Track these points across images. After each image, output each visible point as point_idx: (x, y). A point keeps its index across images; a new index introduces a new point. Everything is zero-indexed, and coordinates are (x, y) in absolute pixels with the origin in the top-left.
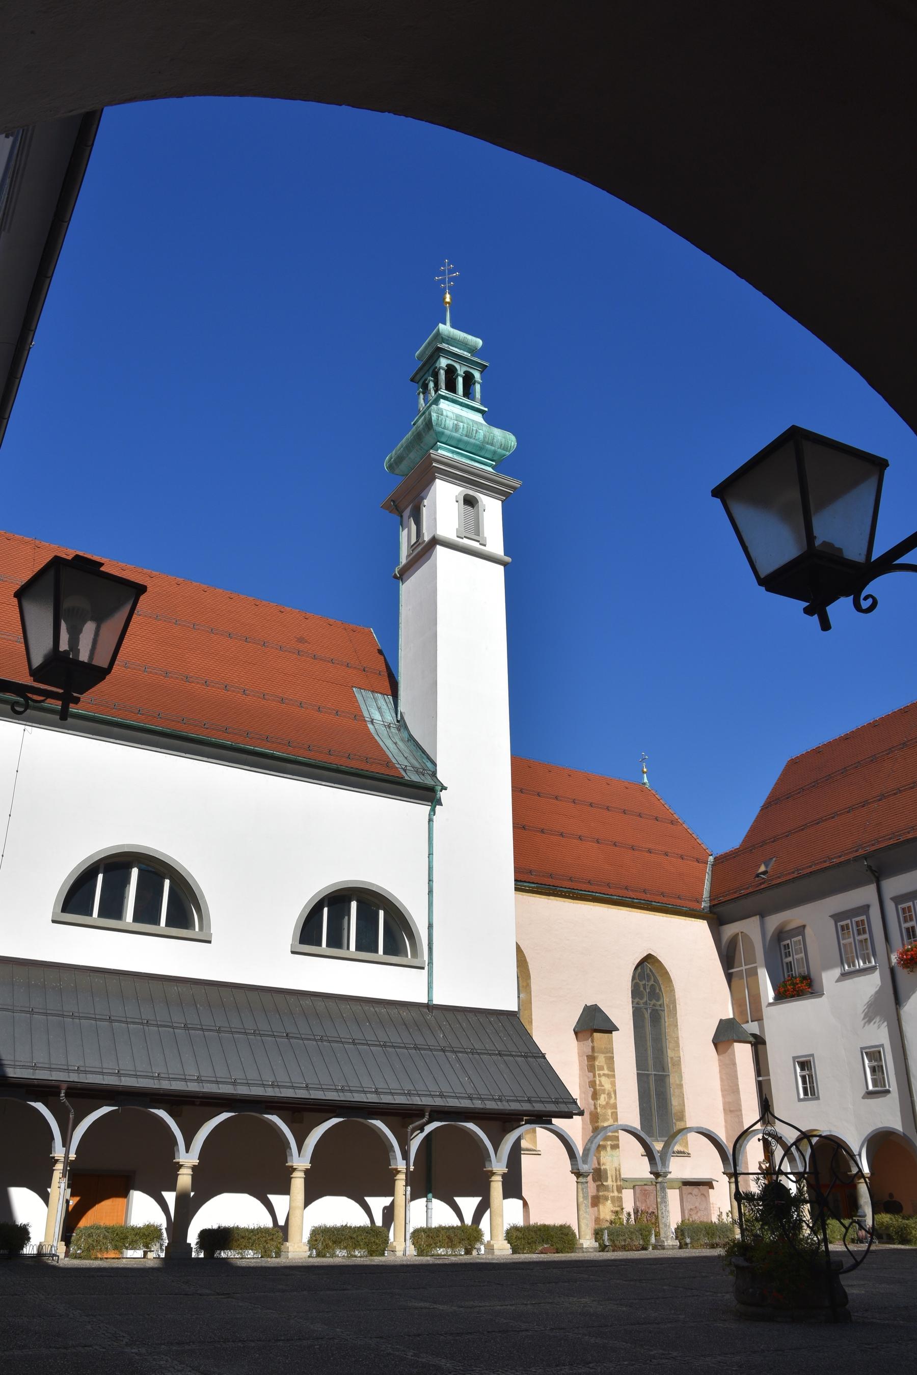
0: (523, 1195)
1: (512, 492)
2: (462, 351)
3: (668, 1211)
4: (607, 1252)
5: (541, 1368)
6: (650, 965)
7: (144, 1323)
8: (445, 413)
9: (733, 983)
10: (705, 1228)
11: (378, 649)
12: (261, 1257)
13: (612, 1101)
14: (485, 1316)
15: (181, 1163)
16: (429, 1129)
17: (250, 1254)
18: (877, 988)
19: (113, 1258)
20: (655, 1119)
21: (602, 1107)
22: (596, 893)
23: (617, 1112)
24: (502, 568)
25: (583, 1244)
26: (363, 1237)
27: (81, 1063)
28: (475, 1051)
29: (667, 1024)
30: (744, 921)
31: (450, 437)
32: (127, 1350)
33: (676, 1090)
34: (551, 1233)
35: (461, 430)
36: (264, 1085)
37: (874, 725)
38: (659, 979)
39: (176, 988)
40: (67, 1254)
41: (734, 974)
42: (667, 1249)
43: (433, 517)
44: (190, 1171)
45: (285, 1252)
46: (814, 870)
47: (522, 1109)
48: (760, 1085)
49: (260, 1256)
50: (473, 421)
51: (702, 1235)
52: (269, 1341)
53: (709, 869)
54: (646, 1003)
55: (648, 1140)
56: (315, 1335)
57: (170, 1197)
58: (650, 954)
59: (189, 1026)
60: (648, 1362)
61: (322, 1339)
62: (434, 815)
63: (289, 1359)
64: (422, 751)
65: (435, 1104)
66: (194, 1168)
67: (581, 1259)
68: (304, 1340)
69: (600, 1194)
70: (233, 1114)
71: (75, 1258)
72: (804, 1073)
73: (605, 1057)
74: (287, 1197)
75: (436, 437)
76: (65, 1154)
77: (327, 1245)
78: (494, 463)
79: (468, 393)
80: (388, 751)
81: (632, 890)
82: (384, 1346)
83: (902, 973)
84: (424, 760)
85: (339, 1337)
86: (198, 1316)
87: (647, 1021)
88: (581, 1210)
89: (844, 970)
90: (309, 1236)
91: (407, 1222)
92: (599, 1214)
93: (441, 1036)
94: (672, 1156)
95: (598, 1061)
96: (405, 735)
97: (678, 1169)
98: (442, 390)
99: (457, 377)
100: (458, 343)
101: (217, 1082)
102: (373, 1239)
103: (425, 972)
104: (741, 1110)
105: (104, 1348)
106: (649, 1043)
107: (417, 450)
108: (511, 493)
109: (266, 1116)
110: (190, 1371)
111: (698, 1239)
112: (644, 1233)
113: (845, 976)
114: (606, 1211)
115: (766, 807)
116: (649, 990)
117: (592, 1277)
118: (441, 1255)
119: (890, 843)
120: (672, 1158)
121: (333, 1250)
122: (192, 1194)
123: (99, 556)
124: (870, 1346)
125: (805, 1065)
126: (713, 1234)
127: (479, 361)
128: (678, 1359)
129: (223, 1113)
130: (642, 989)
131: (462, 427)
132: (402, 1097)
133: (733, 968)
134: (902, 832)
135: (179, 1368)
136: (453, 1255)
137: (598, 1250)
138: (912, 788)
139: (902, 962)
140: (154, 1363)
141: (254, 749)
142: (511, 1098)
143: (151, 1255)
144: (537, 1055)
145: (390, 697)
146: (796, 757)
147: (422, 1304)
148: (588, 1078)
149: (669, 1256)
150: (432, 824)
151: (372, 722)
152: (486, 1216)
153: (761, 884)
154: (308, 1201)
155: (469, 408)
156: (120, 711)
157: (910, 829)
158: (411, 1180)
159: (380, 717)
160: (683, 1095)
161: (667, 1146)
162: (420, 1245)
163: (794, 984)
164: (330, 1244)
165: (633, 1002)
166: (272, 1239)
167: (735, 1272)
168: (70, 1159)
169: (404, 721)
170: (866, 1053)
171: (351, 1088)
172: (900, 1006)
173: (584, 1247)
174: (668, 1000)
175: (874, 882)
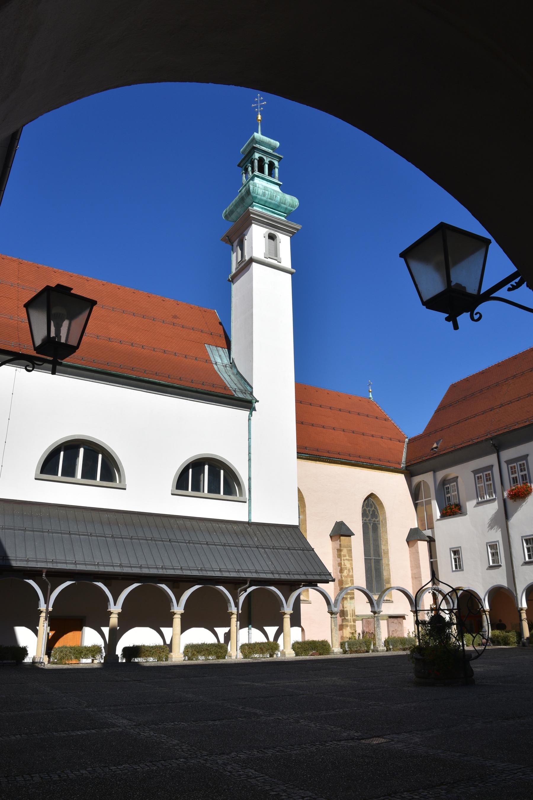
1: (296, 232)
4: (347, 654)
9: (418, 509)
10: (400, 640)
11: (219, 322)
13: (351, 574)
16: (249, 590)
17: (151, 659)
18: (496, 510)
19: (75, 664)
20: (374, 583)
21: (345, 577)
22: (343, 459)
23: (353, 579)
24: (290, 276)
27: (54, 558)
28: (275, 548)
31: (261, 200)
32: (86, 710)
33: (386, 567)
35: (267, 196)
36: (157, 568)
37: (498, 365)
38: (377, 506)
39: (106, 515)
40: (49, 662)
41: (418, 504)
42: (380, 652)
44: (117, 616)
48: (432, 563)
49: (157, 661)
52: (164, 703)
53: (405, 446)
54: (370, 520)
55: (370, 594)
57: (106, 630)
58: (372, 493)
59: (114, 536)
61: (192, 701)
62: (252, 416)
64: (245, 381)
65: (252, 577)
68: (183, 702)
69: (344, 623)
70: (140, 584)
71: (54, 664)
73: (347, 550)
74: (171, 629)
75: (252, 199)
76: (46, 608)
77: (193, 654)
78: (286, 215)
79: (271, 174)
83: (510, 502)
84: (245, 385)
89: (479, 501)
91: (238, 640)
92: (343, 634)
94: (383, 603)
96: (235, 371)
98: (256, 172)
99: (265, 164)
101: (131, 567)
102: (219, 650)
105: (73, 709)
106: (371, 542)
112: (367, 643)
113: (479, 504)
114: (347, 633)
116: (372, 513)
118: (256, 658)
119: (505, 431)
121: (197, 656)
122: (118, 628)
125: (456, 552)
126: (405, 643)
127: (277, 155)
129: (134, 583)
130: (368, 512)
131: (267, 194)
136: (263, 658)
138: (518, 400)
139: (510, 496)
144: (309, 549)
145: (226, 350)
147: (246, 683)
148: (338, 561)
151: (216, 364)
152: (281, 636)
153: (434, 454)
154: (183, 630)
155: (271, 183)
158: (240, 618)
160: (390, 570)
161: (380, 597)
162: (245, 653)
163: (451, 509)
164: (195, 653)
165: (362, 519)
166: (163, 651)
168: (49, 610)
169: (234, 363)
170: (489, 545)
171: (206, 569)
172: (508, 520)
173: (335, 652)
174: (382, 518)
175: (496, 452)
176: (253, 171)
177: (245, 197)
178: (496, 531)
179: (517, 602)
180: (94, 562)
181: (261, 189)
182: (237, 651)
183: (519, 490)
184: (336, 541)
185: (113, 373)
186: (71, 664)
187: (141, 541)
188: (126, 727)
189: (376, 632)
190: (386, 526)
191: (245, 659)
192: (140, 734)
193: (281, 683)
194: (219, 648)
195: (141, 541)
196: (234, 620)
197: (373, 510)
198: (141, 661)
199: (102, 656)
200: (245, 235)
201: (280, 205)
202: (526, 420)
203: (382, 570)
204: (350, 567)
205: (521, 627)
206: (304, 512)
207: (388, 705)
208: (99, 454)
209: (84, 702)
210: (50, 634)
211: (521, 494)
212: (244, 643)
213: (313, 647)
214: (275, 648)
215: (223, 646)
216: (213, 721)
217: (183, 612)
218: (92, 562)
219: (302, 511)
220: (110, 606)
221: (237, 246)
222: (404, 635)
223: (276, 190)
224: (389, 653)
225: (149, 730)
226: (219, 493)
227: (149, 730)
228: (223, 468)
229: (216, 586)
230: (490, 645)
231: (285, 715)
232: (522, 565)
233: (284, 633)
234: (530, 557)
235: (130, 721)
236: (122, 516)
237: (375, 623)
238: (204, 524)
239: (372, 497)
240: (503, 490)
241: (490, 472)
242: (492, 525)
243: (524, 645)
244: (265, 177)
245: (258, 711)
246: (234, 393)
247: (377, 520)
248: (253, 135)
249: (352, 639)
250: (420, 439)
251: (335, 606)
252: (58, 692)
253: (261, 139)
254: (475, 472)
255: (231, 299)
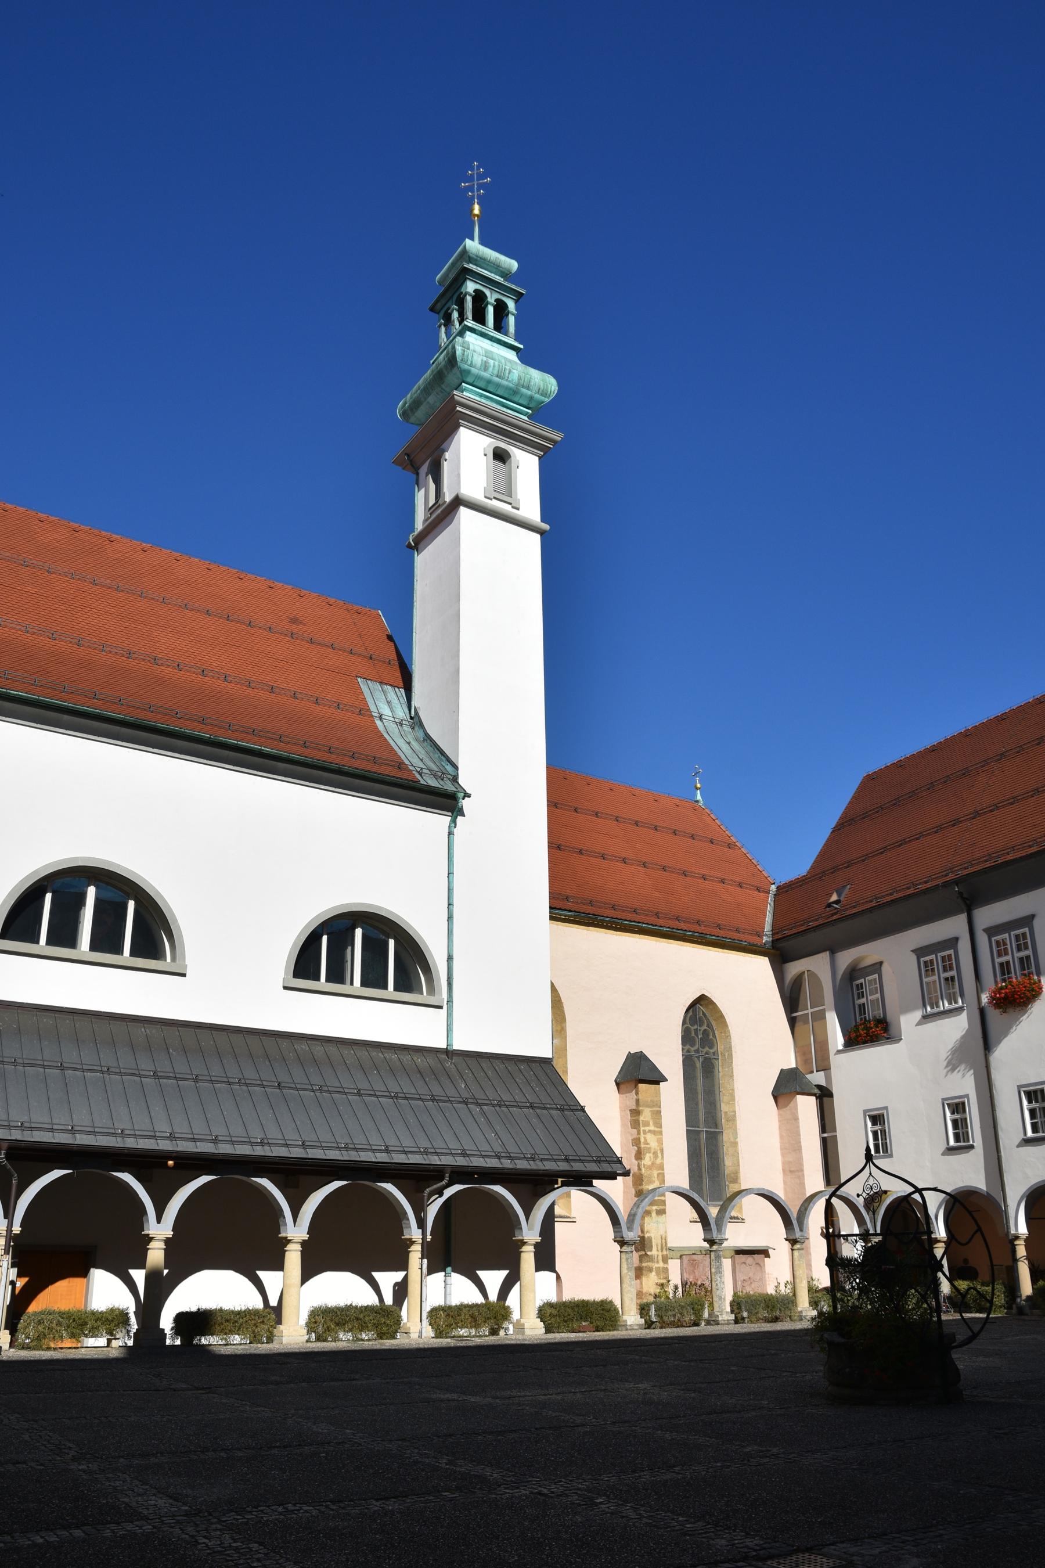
0: (557, 1269)
1: (552, 446)
2: (493, 275)
3: (723, 1283)
4: (654, 1328)
5: (614, 1476)
6: (702, 1007)
7: (99, 1428)
8: (471, 347)
9: (797, 1029)
10: (765, 1300)
11: (387, 635)
12: (250, 1343)
13: (658, 1161)
14: (527, 1408)
15: (151, 1236)
16: (449, 1192)
17: (236, 1339)
18: (962, 1032)
19: (70, 1348)
20: (706, 1180)
21: (647, 1168)
22: (643, 923)
23: (664, 1173)
24: (538, 537)
25: (626, 1321)
26: (371, 1318)
27: (26, 1118)
28: (503, 1103)
29: (721, 1074)
30: (811, 957)
31: (479, 377)
32: (72, 1467)
33: (730, 1149)
34: (591, 1309)
35: (491, 369)
36: (251, 1143)
37: (966, 735)
38: (713, 1023)
39: (143, 1030)
40: (12, 1345)
41: (798, 1018)
42: (722, 1324)
43: (457, 473)
44: (162, 1245)
45: (279, 1336)
46: (896, 897)
47: (558, 1169)
48: (824, 1142)
49: (248, 1342)
50: (506, 359)
51: (761, 1308)
52: (261, 1448)
53: (771, 899)
54: (697, 1051)
55: (703, 1204)
56: (319, 1439)
57: (139, 1276)
58: (703, 995)
59: (159, 1074)
60: (746, 1462)
61: (328, 1443)
62: (455, 827)
63: (287, 1473)
64: (441, 753)
65: (456, 1164)
66: (167, 1241)
67: (626, 1337)
68: (305, 1445)
69: (644, 1265)
70: (215, 1177)
71: (23, 1348)
72: (876, 1128)
73: (651, 1111)
74: (280, 1273)
75: (460, 376)
76: (7, 1227)
77: (328, 1327)
78: (530, 412)
79: (500, 325)
80: (400, 751)
81: (684, 922)
82: (409, 1451)
83: (993, 1014)
84: (442, 763)
85: (351, 1441)
86: (170, 1418)
87: (699, 1071)
88: (625, 1283)
89: (926, 1012)
90: (307, 1317)
91: (424, 1299)
92: (642, 1288)
93: (463, 1086)
94: (730, 1222)
95: (643, 1116)
96: (420, 734)
97: (735, 1236)
98: (467, 320)
99: (486, 306)
100: (488, 265)
101: (194, 1140)
102: (383, 1320)
103: (443, 1012)
104: (802, 1170)
105: (42, 1465)
106: (701, 1096)
107: (437, 393)
108: (551, 448)
109: (254, 1179)
110: (154, 1495)
111: (756, 1313)
112: (696, 1307)
113: (926, 1018)
114: (650, 1284)
115: (837, 829)
116: (702, 1036)
117: (643, 1358)
118: (463, 1336)
119: (986, 866)
120: (729, 1223)
121: (336, 1333)
122: (166, 1272)
123: (45, 514)
124: (1002, 1431)
125: (877, 1119)
126: (774, 1307)
127: (513, 287)
128: (781, 1457)
129: (201, 1176)
130: (693, 1034)
131: (492, 365)
132: (418, 1156)
133: (796, 1011)
134: (999, 853)
135: (141, 1490)
136: (477, 1336)
137: (644, 1327)
138: (1012, 804)
139: (994, 1002)
140: (107, 1484)
141: (237, 744)
142: (546, 1157)
143: (115, 1344)
144: (575, 1108)
145: (402, 690)
146: (873, 773)
147: (448, 1396)
148: (632, 1135)
149: (726, 1332)
150: (452, 838)
151: (380, 718)
152: (516, 1290)
153: (833, 915)
154: (306, 1277)
155: (501, 344)
156: (71, 695)
157: (1009, 850)
158: (428, 1251)
159: (390, 712)
160: (738, 1154)
161: (723, 1209)
162: (439, 1325)
163: (868, 1029)
164: (332, 1326)
165: (683, 1049)
166: (263, 1321)
167: (827, 1349)
168: (13, 1232)
169: (419, 717)
170: (947, 1104)
171: (357, 1146)
172: (989, 1052)
173: (628, 1323)
174: (722, 1047)
175: (965, 911)
176: (462, 318)
177: (444, 371)
178: (964, 1075)
179: (1007, 1223)
180: (114, 1129)
181: (480, 355)
182: (421, 1321)
183: (1015, 988)
184: (629, 1092)
185: (161, 727)
186: (60, 1348)
187: (217, 1086)
188: (164, 1519)
189: (713, 1283)
190: (732, 1062)
191: (439, 1340)
192: (196, 1541)
193: (526, 1396)
194: (383, 1316)
195: (217, 1085)
196: (415, 1257)
197: (705, 1030)
198: (215, 1343)
199: (130, 1331)
200: (444, 451)
201: (518, 389)
202: (1030, 843)
203: (721, 1153)
204: (658, 1146)
205: (1016, 1274)
206: (563, 1032)
207: (793, 1455)
208: (130, 901)
209: (71, 1445)
210: (19, 1285)
211: (1018, 997)
212: (437, 1305)
213: (584, 1315)
214: (503, 1316)
215: (392, 1312)
216: (381, 1499)
217: (307, 1239)
218: (111, 1128)
219: (557, 1030)
220: (147, 1224)
221: (427, 475)
222: (766, 1289)
223: (509, 359)
224: (742, 1327)
225: (220, 1530)
226: (385, 987)
227: (220, 1530)
228: (395, 936)
229: (378, 1184)
230: (947, 1311)
231: (555, 1484)
232: (1018, 1146)
233: (522, 1284)
234: (1035, 1129)
235: (175, 1500)
236: (177, 1033)
237: (712, 1263)
238: (352, 1052)
239: (702, 1003)
240: (979, 992)
241: (951, 952)
242: (954, 1062)
243: (1021, 1311)
244: (487, 332)
245: (488, 1472)
246: (419, 778)
247: (712, 1051)
248: (464, 243)
249: (659, 1297)
250: (801, 886)
251: (630, 1229)
252: (16, 1417)
253: (480, 254)
254: (919, 952)
255: (414, 584)
